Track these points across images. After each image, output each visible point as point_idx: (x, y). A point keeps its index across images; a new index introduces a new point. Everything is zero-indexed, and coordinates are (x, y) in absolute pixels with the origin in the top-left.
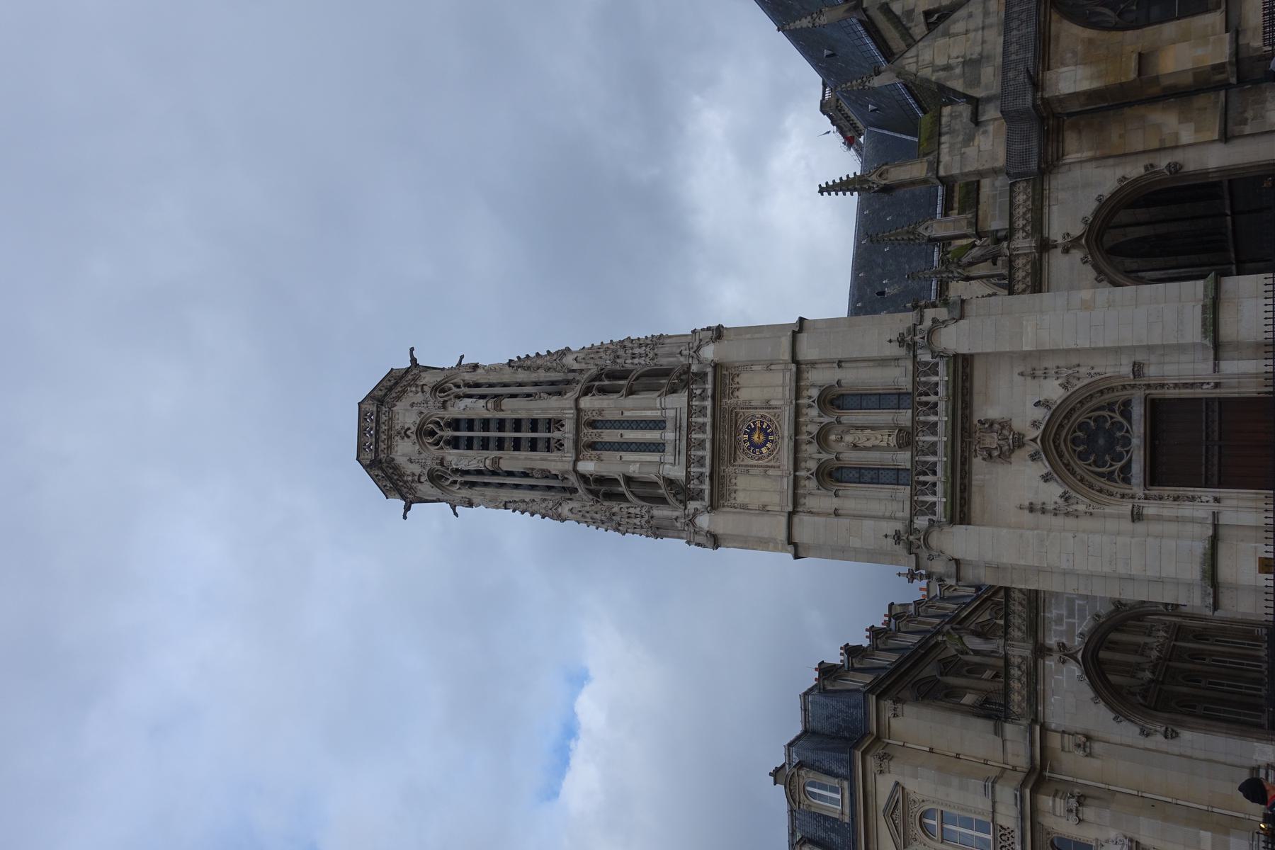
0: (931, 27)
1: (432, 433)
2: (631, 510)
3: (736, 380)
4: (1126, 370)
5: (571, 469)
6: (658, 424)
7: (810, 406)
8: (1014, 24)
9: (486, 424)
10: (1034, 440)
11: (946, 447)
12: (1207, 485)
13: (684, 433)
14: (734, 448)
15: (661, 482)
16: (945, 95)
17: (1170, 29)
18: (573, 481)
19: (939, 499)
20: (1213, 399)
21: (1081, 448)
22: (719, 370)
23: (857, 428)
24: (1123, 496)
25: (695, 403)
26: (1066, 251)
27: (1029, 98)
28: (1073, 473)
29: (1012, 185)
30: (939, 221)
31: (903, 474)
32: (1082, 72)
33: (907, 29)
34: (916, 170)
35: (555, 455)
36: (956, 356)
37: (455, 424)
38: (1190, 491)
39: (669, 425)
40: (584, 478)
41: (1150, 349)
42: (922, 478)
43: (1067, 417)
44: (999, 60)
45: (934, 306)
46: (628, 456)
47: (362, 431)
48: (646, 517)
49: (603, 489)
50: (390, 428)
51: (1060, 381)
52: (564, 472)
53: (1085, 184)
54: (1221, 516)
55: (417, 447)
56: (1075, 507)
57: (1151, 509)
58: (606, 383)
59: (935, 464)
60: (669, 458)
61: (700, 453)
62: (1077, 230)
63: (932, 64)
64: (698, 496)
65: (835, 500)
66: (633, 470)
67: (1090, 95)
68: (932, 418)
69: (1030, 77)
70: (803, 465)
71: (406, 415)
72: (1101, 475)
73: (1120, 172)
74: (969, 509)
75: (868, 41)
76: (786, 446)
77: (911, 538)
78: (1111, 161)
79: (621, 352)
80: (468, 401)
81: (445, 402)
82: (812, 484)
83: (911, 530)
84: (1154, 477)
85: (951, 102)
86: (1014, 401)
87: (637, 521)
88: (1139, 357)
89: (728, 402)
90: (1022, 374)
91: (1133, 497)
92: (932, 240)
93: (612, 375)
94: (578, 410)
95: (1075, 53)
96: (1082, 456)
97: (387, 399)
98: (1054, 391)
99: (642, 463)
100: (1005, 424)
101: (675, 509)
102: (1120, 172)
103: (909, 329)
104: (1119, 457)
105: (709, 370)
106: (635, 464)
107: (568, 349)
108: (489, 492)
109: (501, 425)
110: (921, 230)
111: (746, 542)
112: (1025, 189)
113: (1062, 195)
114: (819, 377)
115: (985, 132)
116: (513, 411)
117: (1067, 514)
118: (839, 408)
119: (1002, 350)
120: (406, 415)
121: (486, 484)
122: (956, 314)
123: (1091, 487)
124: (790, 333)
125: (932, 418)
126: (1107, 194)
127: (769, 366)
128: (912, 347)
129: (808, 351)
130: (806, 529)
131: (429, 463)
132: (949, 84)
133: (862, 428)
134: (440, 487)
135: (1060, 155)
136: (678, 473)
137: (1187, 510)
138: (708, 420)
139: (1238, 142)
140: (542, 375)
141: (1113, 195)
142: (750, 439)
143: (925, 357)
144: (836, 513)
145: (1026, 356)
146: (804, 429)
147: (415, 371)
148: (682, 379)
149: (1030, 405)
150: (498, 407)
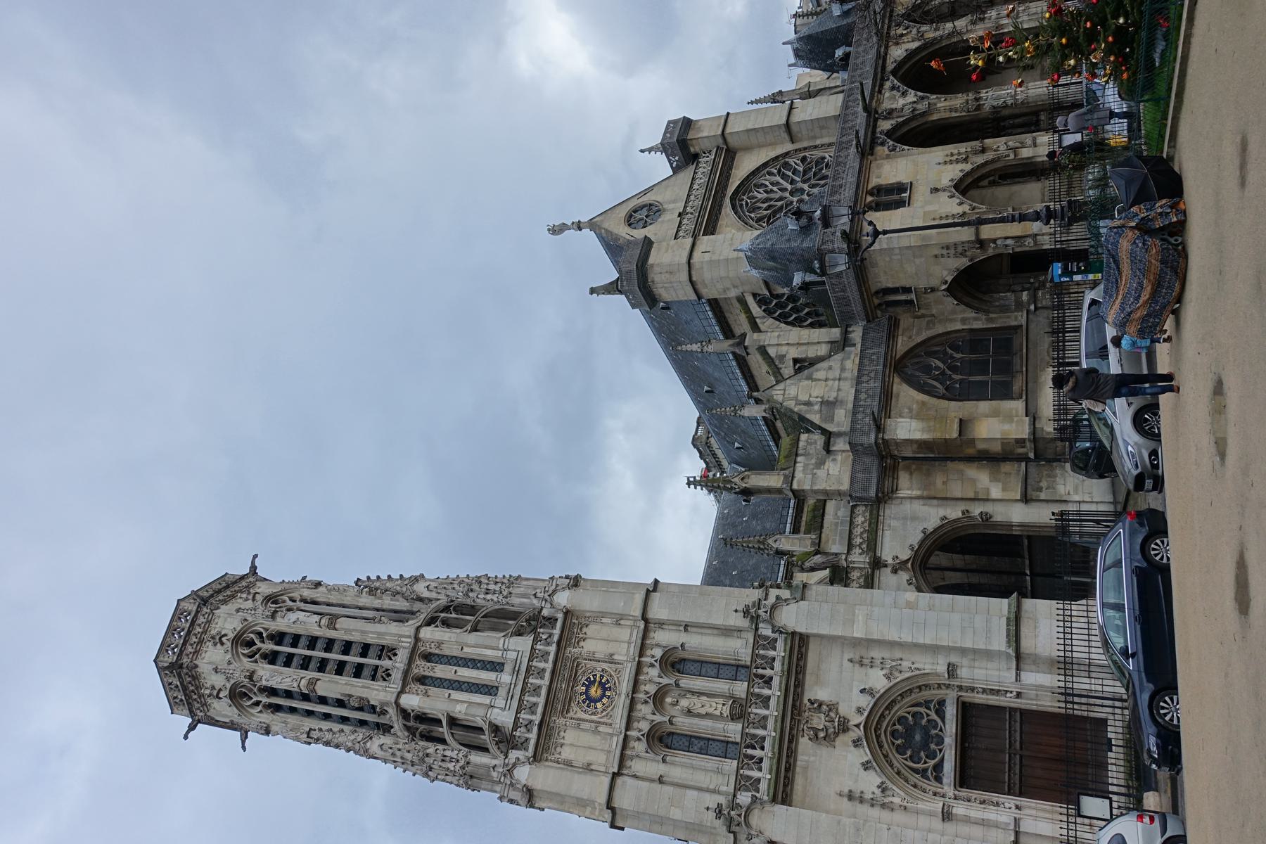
0: (798, 371)
1: (251, 644)
2: (448, 753)
3: (584, 630)
4: (942, 668)
5: (393, 700)
6: (497, 666)
7: (652, 665)
8: (865, 379)
9: (313, 642)
10: (858, 726)
11: (776, 721)
12: (1010, 792)
13: (522, 677)
14: (569, 699)
15: (486, 727)
16: (801, 424)
17: (984, 406)
18: (392, 716)
19: (764, 775)
20: (1015, 709)
21: (899, 742)
22: (569, 616)
23: (693, 693)
24: (935, 794)
25: (539, 646)
26: (895, 571)
27: (873, 436)
28: (891, 765)
29: (854, 507)
30: (787, 537)
31: (731, 748)
32: (915, 424)
33: (779, 369)
34: (773, 480)
35: (380, 684)
36: (794, 633)
37: (279, 638)
38: (995, 797)
39: (508, 668)
40: (404, 713)
41: (963, 651)
42: (750, 751)
43: (889, 708)
44: (850, 406)
45: (778, 587)
46: (457, 695)
47: (171, 630)
48: (462, 763)
49: (422, 727)
50: (205, 632)
51: (884, 672)
52: (383, 704)
53: (911, 520)
54: (1022, 823)
55: (229, 656)
56: (891, 799)
57: (959, 809)
58: (454, 615)
59: (763, 739)
60: (500, 701)
61: (534, 699)
62: (905, 555)
63: (796, 398)
64: (523, 745)
65: (683, 634)
66: (459, 711)
67: (923, 445)
68: (766, 692)
69: (874, 419)
70: (635, 725)
71: (227, 621)
72: (916, 771)
73: (942, 512)
74: (792, 789)
75: (742, 382)
76: (621, 703)
77: (732, 813)
78: (935, 502)
79: (476, 587)
80: (301, 615)
81: (275, 612)
82: (640, 747)
83: (733, 805)
84: (965, 779)
85: (808, 431)
86: (843, 686)
87: (451, 766)
88: (954, 659)
89: (572, 651)
90: (851, 660)
91: (943, 796)
92: (780, 553)
93: (461, 609)
94: (417, 639)
95: (911, 410)
96: (900, 750)
97: (212, 600)
98: (878, 681)
99: (470, 704)
100: (832, 707)
101: (495, 757)
102: (942, 512)
103: (754, 603)
104: (931, 755)
105: (560, 616)
106: (463, 705)
107: (422, 576)
108: (293, 719)
109: (329, 645)
110: (770, 541)
111: (564, 802)
112: (864, 512)
113: (894, 523)
114: (665, 638)
115: (834, 460)
116: (346, 631)
117: (883, 806)
118: (667, 747)
119: (835, 633)
120: (227, 621)
121: (293, 710)
122: (798, 595)
123: (907, 781)
124: (643, 592)
125: (766, 692)
126: (931, 529)
127: (619, 620)
128: (755, 619)
129: (658, 611)
130: (629, 794)
131: (237, 674)
132: (808, 416)
133: (700, 694)
134: (240, 707)
135: (894, 490)
136: (505, 718)
137: (991, 814)
138: (549, 666)
139: (1034, 504)
140: (387, 602)
141: (935, 530)
142: (587, 692)
143: (766, 630)
144: (661, 780)
145: (856, 643)
146: (642, 688)
147: (251, 579)
148: (533, 623)
149: (856, 691)
150: (332, 626)
